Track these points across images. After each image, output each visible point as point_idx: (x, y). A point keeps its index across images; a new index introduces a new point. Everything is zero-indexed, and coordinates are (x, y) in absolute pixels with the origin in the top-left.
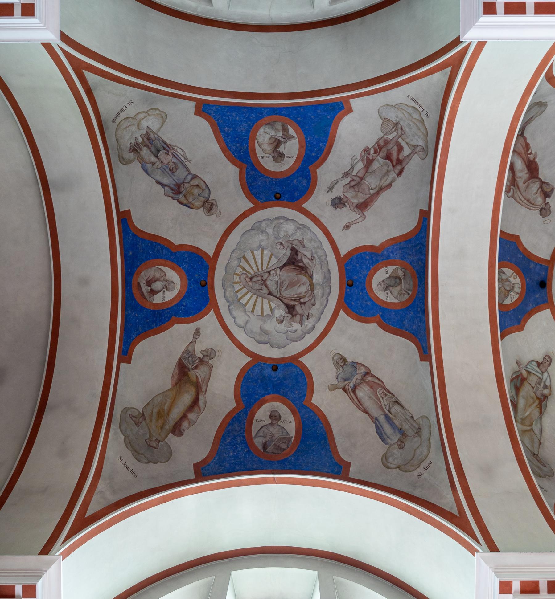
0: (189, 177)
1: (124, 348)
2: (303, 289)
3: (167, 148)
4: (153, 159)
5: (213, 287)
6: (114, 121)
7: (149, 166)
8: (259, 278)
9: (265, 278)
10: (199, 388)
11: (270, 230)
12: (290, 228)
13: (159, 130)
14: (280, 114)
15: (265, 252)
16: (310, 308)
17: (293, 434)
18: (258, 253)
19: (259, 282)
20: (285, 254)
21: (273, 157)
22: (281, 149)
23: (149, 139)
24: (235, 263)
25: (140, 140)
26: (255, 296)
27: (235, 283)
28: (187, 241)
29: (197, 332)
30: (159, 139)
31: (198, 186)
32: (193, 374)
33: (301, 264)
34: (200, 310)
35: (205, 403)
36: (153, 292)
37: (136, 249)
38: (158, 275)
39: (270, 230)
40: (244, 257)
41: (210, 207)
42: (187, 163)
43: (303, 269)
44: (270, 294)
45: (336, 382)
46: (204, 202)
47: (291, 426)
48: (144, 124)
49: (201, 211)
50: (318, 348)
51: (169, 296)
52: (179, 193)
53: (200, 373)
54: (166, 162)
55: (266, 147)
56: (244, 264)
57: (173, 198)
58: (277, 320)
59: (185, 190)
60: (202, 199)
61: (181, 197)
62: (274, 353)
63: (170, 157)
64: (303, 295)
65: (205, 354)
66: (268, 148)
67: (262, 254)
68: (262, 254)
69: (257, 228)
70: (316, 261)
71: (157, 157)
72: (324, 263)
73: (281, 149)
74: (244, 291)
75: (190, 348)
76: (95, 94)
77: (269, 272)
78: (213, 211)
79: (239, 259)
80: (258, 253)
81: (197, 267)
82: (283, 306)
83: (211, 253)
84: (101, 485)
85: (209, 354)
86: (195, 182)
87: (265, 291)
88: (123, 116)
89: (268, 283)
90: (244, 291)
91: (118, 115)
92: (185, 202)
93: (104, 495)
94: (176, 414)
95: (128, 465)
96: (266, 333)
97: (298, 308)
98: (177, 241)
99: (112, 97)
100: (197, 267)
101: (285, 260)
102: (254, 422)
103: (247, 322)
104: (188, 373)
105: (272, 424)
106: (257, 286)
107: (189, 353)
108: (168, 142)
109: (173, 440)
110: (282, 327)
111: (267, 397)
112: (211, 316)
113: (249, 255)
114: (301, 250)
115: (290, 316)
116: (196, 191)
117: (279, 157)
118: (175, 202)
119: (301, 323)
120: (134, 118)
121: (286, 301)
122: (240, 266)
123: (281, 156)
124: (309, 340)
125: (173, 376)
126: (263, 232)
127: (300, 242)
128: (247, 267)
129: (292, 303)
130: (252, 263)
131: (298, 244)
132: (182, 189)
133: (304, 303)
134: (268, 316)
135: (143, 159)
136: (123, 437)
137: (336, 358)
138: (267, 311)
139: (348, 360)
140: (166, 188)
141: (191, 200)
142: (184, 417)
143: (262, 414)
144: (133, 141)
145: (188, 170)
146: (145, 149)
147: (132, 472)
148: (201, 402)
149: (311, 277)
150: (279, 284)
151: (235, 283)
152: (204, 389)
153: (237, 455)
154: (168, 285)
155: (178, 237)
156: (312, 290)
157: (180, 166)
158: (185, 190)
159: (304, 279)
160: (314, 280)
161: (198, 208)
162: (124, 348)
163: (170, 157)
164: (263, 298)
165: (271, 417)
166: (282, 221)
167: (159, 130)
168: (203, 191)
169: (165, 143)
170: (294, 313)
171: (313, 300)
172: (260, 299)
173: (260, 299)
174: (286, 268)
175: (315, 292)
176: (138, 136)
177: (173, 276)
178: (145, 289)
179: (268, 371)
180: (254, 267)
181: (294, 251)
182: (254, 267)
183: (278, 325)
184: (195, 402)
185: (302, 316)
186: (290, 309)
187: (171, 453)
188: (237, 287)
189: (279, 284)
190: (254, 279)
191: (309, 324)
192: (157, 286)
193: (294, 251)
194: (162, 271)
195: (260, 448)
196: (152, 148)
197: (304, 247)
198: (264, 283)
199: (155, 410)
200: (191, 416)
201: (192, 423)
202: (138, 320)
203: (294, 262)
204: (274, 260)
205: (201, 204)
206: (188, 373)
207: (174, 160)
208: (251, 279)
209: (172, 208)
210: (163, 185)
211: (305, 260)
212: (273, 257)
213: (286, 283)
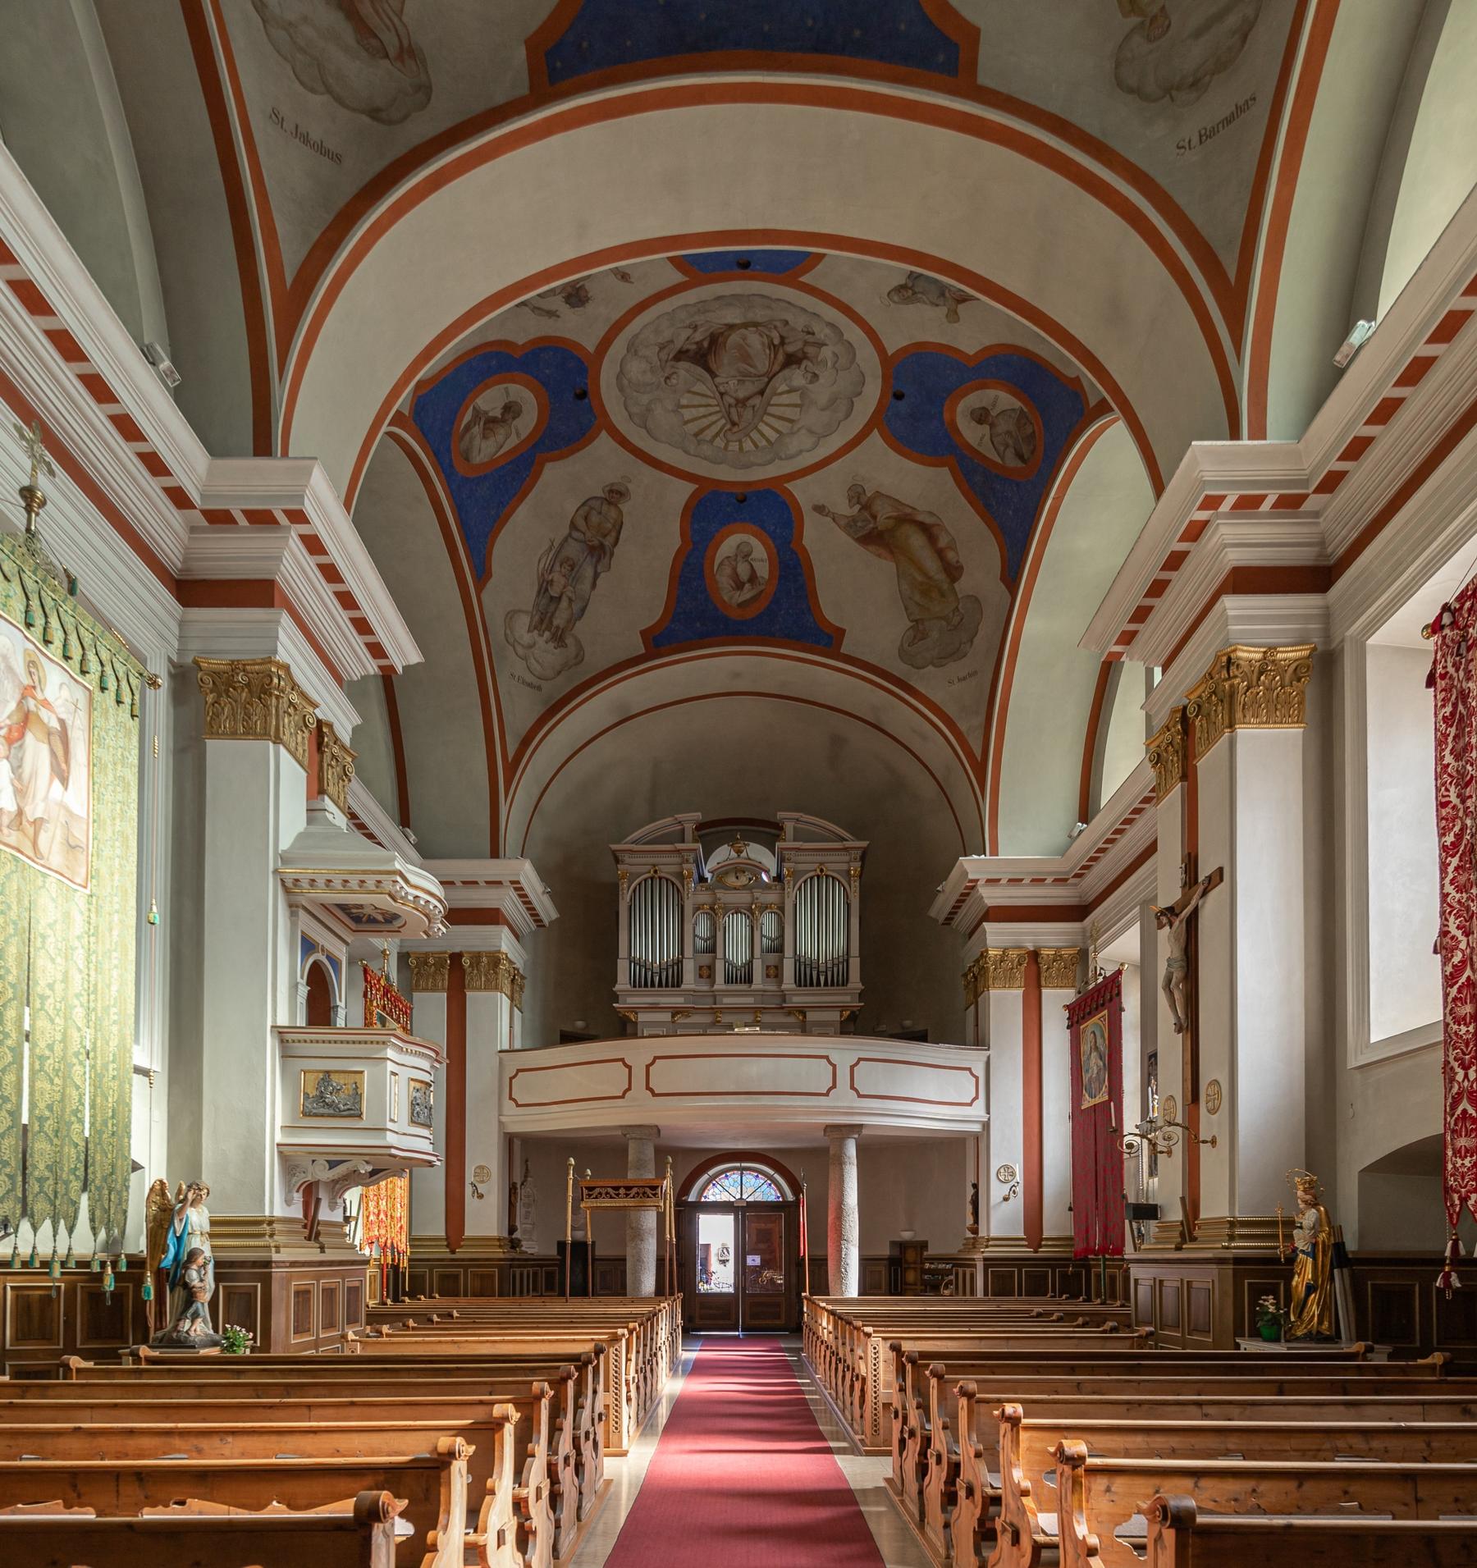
0: (576, 534)
1: (822, 639)
2: (755, 341)
3: (544, 586)
4: (564, 603)
5: (748, 484)
6: (539, 688)
7: (576, 607)
8: (733, 410)
9: (732, 401)
10: (906, 518)
11: (645, 399)
12: (636, 369)
13: (526, 612)
14: (452, 466)
15: (684, 402)
16: (793, 329)
17: (1018, 404)
18: (688, 414)
19: (738, 414)
20: (687, 371)
21: (514, 418)
22: (497, 413)
23: (542, 621)
24: (706, 449)
25: (547, 634)
26: (766, 418)
27: (741, 448)
28: (675, 527)
29: (820, 509)
30: (536, 605)
31: (586, 518)
32: (882, 522)
33: (706, 344)
34: (784, 503)
35: (931, 513)
36: (753, 578)
37: (692, 619)
38: (728, 570)
39: (645, 399)
40: (696, 435)
41: (615, 495)
42: (556, 544)
43: (715, 341)
44: (762, 393)
45: (945, 310)
46: (610, 503)
47: (1003, 400)
48: (527, 638)
49: (625, 507)
50: (873, 323)
51: (759, 551)
52: (602, 546)
53: (884, 512)
54: (563, 581)
55: (500, 438)
56: (708, 434)
57: (612, 554)
58: (811, 382)
59: (595, 537)
60: (605, 507)
61: (608, 542)
62: (873, 392)
63: (556, 576)
64: (766, 341)
65: (855, 500)
66: (501, 432)
67: (687, 407)
68: (687, 407)
69: (643, 421)
70: (699, 319)
71: (560, 598)
72: (702, 307)
73: (497, 413)
74: (755, 435)
75: (843, 522)
76: (524, 733)
77: (722, 394)
78: (623, 489)
79: (699, 443)
80: (688, 414)
81: (713, 508)
82: (786, 372)
83: (689, 488)
84: (963, 726)
85: (856, 494)
86: (581, 523)
87: (757, 401)
88: (529, 678)
89: (741, 395)
90: (755, 435)
91: (530, 685)
92: (614, 534)
93: (969, 725)
94: (932, 565)
95: (961, 675)
96: (833, 401)
97: (790, 349)
98: (677, 542)
99: (519, 711)
100: (713, 508)
101: (700, 370)
102: (980, 449)
103: (810, 431)
104: (880, 529)
105: (992, 426)
106: (748, 414)
107: (850, 525)
108: (536, 588)
109: (964, 586)
110: (826, 376)
111: (946, 416)
112: (796, 488)
113: (692, 428)
114: (678, 345)
115: (805, 363)
116: (595, 519)
117: (511, 410)
118: (616, 550)
119: (821, 345)
120: (525, 658)
121: (776, 367)
122: (711, 441)
123: (507, 408)
124: (854, 334)
125: (879, 556)
126: (649, 410)
127: (661, 349)
128: (715, 429)
129: (781, 358)
130: (706, 422)
131: (666, 351)
132: (596, 543)
133: (782, 338)
134: (802, 396)
135: (569, 621)
136: (930, 667)
137: (896, 298)
138: (795, 398)
139: (903, 282)
140: (599, 569)
141: (609, 526)
142: (940, 554)
143: (972, 433)
144: (551, 645)
145: (565, 540)
146: (556, 622)
147: (970, 675)
148: (928, 520)
149: (731, 327)
150: (743, 377)
151: (741, 448)
152: (909, 511)
153: (1015, 504)
154: (743, 550)
155: (670, 539)
156: (756, 325)
157: (564, 554)
158: (595, 537)
159: (734, 338)
160: (737, 321)
161: (621, 512)
162: (822, 639)
163: (556, 576)
164: (769, 404)
165: (980, 422)
166: (625, 382)
167: (526, 612)
168: (592, 508)
169: (539, 592)
170: (800, 355)
171: (778, 324)
172: (771, 410)
173: (771, 410)
174: (713, 366)
175: (760, 320)
176: (542, 641)
177: (729, 545)
178: (747, 593)
179: (902, 406)
180: (714, 418)
181: (681, 355)
182: (714, 418)
183: (822, 381)
184: (926, 529)
185: (806, 343)
186: (792, 360)
187: (977, 599)
188: (748, 445)
189: (743, 377)
190: (736, 418)
191: (822, 333)
192: (743, 571)
193: (681, 355)
194: (721, 564)
195: (1020, 464)
196: (553, 611)
197: (672, 341)
198: (742, 403)
199: (917, 597)
200: (943, 542)
201: (952, 546)
202: (790, 615)
203: (703, 354)
204: (699, 388)
205: (612, 508)
206: (880, 529)
207: (557, 568)
208: (734, 424)
209: (627, 552)
210: (596, 576)
211: (698, 337)
212: (694, 389)
213: (743, 366)
